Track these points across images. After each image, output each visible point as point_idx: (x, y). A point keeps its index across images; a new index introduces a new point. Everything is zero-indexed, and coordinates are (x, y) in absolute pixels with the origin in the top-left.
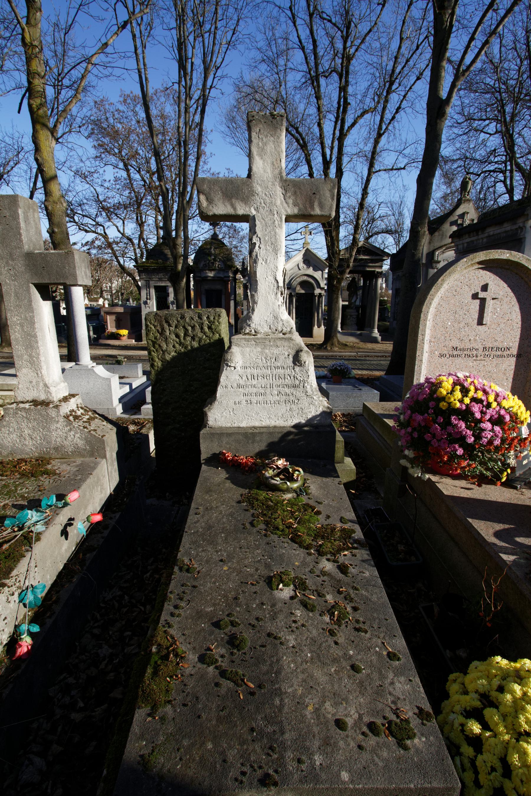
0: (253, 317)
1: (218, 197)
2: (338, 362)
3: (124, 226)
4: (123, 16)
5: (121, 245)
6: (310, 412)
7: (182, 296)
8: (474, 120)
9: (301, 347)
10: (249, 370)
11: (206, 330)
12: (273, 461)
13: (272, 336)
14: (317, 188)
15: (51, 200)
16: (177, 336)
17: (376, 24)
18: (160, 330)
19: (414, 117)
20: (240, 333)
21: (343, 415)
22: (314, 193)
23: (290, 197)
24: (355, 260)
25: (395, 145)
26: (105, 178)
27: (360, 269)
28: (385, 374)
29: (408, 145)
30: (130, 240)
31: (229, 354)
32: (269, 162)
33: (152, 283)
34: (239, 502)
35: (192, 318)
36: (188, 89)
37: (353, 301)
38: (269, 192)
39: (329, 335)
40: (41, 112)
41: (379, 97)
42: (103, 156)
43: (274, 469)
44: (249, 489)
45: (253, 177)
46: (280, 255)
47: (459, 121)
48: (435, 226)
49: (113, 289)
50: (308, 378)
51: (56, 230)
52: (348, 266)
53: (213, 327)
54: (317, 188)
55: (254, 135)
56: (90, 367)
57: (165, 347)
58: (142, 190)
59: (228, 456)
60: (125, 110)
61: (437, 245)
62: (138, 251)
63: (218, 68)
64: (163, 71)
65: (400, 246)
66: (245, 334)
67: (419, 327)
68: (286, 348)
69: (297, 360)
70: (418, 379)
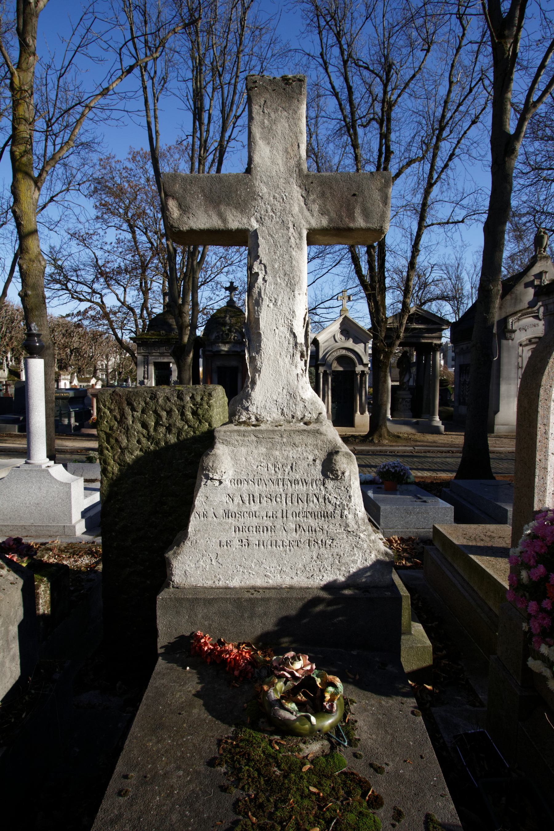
0: (253, 394)
1: (197, 203)
2: (391, 461)
3: (125, 294)
4: (129, 61)
5: (119, 315)
7: (188, 374)
8: (543, 169)
9: (335, 446)
10: (245, 486)
11: (189, 416)
12: (285, 663)
14: (359, 187)
15: (27, 258)
16: (145, 425)
17: (420, 69)
18: (118, 417)
19: (470, 163)
21: (402, 539)
22: (354, 195)
23: (314, 201)
24: (407, 330)
25: (451, 195)
26: (105, 240)
27: (413, 341)
28: (456, 478)
29: (465, 195)
30: (131, 309)
31: (212, 458)
32: (280, 148)
33: (152, 359)
34: (211, 763)
35: (168, 399)
36: (204, 145)
37: (405, 380)
38: (279, 194)
39: (376, 423)
40: (24, 159)
41: (427, 145)
42: (106, 216)
43: (287, 679)
44: (237, 725)
45: (254, 171)
46: (301, 304)
47: (524, 171)
48: (510, 285)
49: (110, 367)
50: (350, 501)
51: (30, 293)
52: (398, 337)
53: (200, 412)
54: (359, 187)
55: (256, 108)
56: (44, 467)
57: (124, 442)
58: (149, 254)
59: (206, 644)
60: (133, 168)
61: (510, 310)
62: (140, 321)
63: (239, 117)
64: (175, 125)
65: (460, 315)
66: (240, 423)
67: (537, 412)
68: (310, 448)
69: (329, 468)
70: (542, 501)
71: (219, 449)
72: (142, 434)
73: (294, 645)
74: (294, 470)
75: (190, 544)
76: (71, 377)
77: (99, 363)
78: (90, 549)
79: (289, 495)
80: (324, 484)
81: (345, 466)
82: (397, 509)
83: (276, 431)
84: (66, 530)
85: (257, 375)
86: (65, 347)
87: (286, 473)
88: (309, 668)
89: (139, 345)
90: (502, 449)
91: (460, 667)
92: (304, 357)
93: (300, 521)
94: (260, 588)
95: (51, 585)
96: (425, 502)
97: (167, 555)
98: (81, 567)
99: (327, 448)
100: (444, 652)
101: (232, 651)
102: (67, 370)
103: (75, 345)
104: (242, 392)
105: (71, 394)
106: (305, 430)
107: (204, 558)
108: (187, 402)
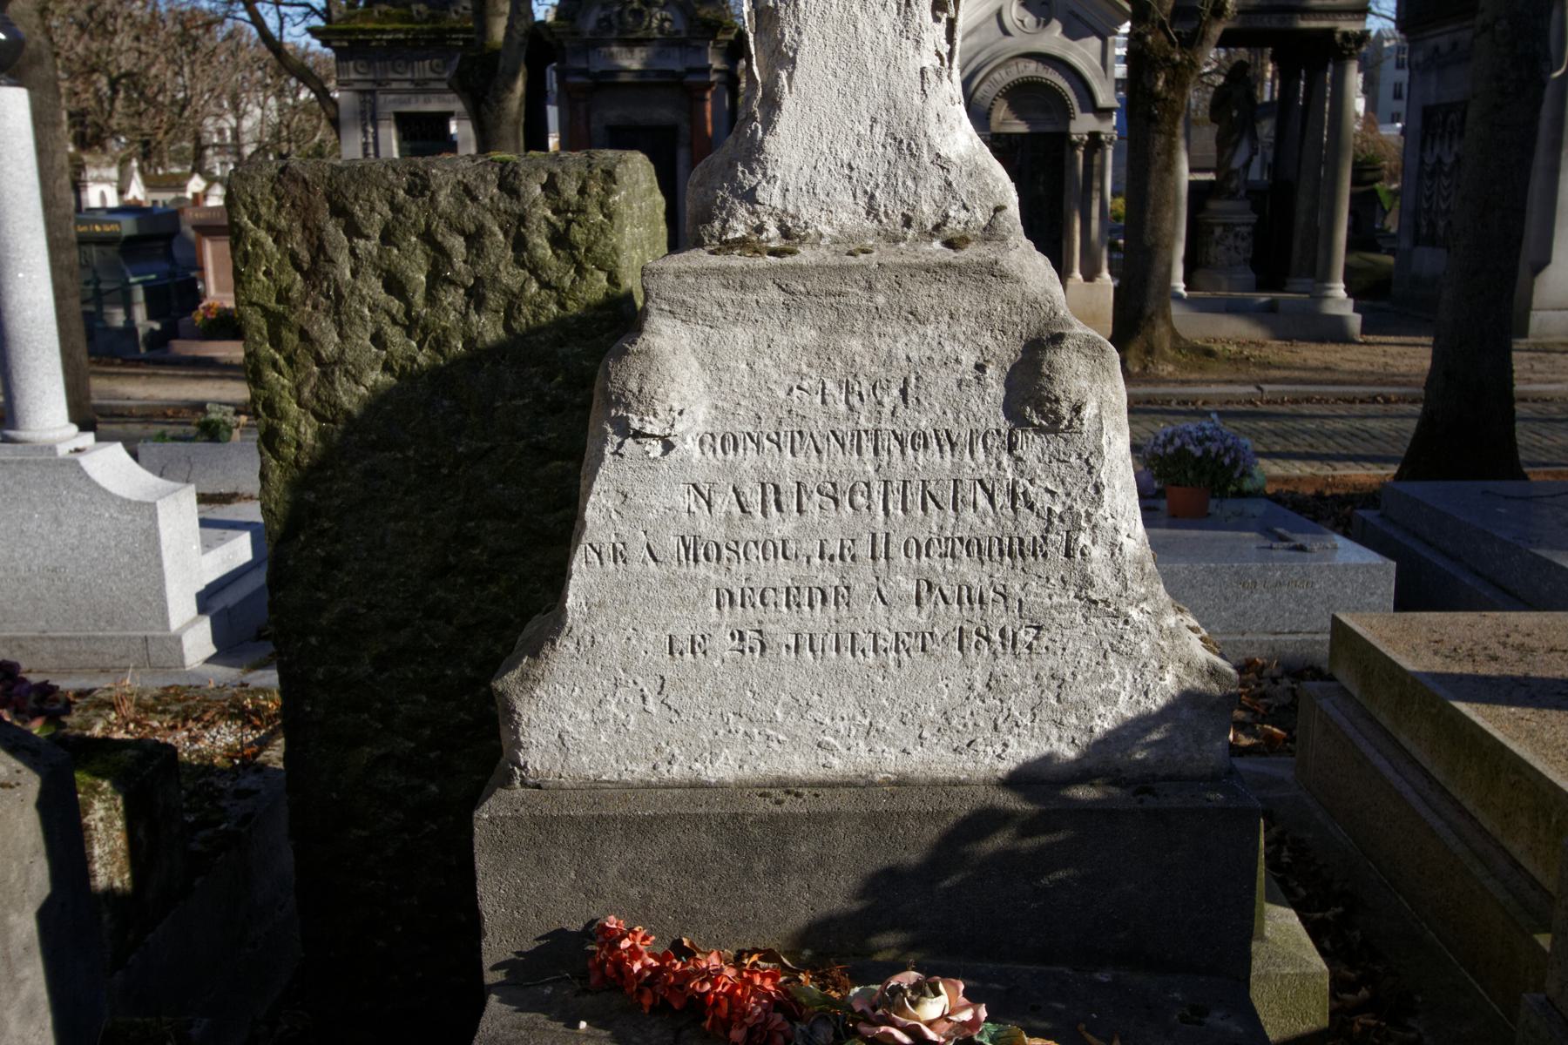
0: (770, 144)
6: (1109, 699)
10: (749, 458)
13: (884, 254)
16: (395, 284)
18: (305, 256)
20: (699, 244)
28: (1398, 477)
31: (636, 365)
33: (389, 104)
37: (1236, 163)
49: (246, 138)
53: (578, 234)
56: (63, 450)
57: (330, 342)
59: (635, 953)
66: (727, 247)
68: (965, 326)
69: (1030, 395)
71: (659, 333)
72: (388, 313)
73: (911, 958)
74: (912, 400)
75: (572, 647)
76: (121, 173)
77: (209, 121)
78: (236, 703)
79: (897, 484)
80: (1011, 448)
81: (1085, 384)
82: (1211, 572)
83: (849, 268)
84: (153, 649)
85: (784, 74)
86: (90, 68)
87: (887, 411)
88: (967, 1016)
89: (341, 55)
90: (1552, 387)
91: (1413, 1035)
92: (945, 10)
93: (932, 568)
94: (803, 784)
95: (126, 803)
96: (1302, 548)
97: (499, 685)
98: (213, 755)
99: (1026, 325)
100: (1364, 993)
101: (719, 972)
102: (104, 149)
103: (126, 63)
104: (730, 140)
105: (127, 226)
106: (948, 265)
107: (621, 692)
108: (535, 204)
